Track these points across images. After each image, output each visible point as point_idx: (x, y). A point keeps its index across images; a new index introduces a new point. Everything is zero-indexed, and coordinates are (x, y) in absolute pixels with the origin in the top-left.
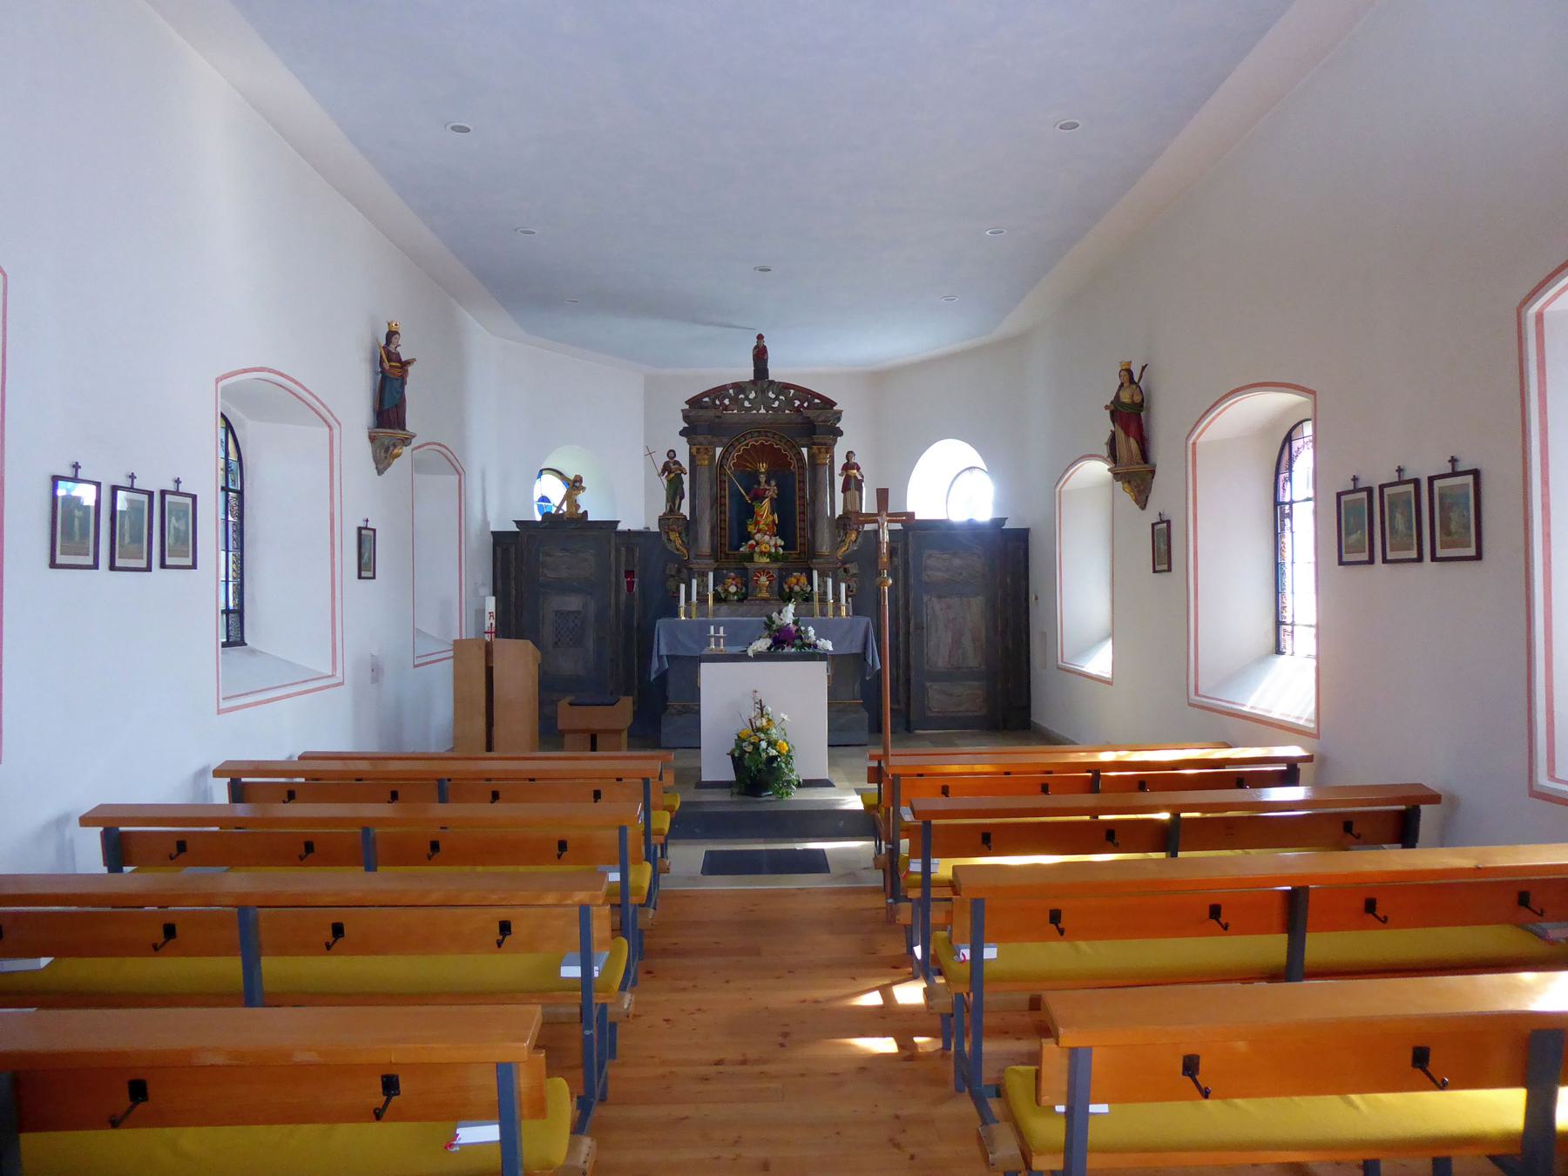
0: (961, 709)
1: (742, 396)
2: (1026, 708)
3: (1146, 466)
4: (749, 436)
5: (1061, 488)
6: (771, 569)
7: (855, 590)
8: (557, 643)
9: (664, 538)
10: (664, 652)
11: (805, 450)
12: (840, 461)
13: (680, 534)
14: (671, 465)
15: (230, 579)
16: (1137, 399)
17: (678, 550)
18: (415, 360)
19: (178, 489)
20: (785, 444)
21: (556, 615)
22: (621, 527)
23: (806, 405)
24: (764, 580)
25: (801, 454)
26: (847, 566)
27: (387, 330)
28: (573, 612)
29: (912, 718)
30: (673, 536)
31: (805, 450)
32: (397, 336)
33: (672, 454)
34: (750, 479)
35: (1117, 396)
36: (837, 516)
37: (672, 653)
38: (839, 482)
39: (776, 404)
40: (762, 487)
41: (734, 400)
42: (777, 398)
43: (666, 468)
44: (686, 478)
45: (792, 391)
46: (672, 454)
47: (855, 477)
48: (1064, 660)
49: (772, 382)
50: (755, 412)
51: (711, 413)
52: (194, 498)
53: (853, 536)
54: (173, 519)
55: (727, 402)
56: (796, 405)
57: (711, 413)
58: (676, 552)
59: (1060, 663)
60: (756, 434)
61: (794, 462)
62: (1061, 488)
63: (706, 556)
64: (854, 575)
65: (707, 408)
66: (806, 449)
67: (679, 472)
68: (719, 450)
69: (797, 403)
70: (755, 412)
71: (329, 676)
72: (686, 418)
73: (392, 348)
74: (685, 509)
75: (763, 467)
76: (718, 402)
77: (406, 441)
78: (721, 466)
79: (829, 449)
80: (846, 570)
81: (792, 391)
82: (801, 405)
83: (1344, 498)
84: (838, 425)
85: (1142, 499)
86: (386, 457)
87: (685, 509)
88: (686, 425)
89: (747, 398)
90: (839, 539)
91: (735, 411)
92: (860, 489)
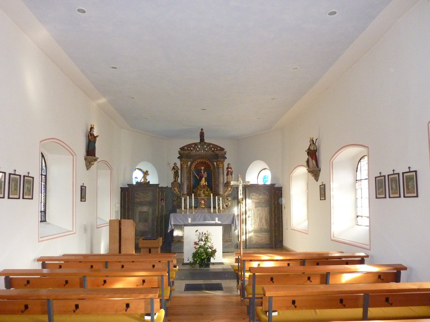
0: (262, 241)
1: (196, 147)
2: (282, 241)
3: (318, 168)
4: (198, 159)
5: (292, 175)
6: (205, 199)
7: (230, 205)
8: (140, 221)
9: (173, 189)
10: (172, 223)
11: (215, 163)
12: (226, 166)
13: (178, 188)
14: (175, 167)
15: (42, 201)
16: (315, 149)
17: (177, 193)
18: (98, 136)
19: (29, 175)
20: (209, 161)
21: (140, 212)
22: (276, 186)
23: (216, 149)
24: (203, 202)
25: (214, 164)
26: (228, 198)
27: (91, 127)
28: (145, 212)
29: (247, 244)
30: (176, 189)
31: (215, 163)
32: (93, 129)
33: (175, 164)
34: (198, 172)
35: (309, 148)
36: (225, 183)
37: (175, 224)
38: (225, 173)
39: (207, 149)
40: (202, 174)
41: (194, 148)
42: (207, 148)
43: (174, 168)
44: (179, 171)
45: (211, 146)
46: (175, 164)
47: (230, 171)
48: (334, 237)
49: (205, 143)
50: (200, 152)
51: (187, 152)
52: (33, 178)
53: (230, 189)
54: (27, 184)
55: (192, 148)
56: (213, 150)
57: (187, 152)
58: (176, 193)
59: (332, 238)
60: (201, 158)
61: (212, 167)
62: (292, 175)
63: (185, 195)
64: (230, 201)
65: (186, 150)
66: (215, 163)
67: (177, 169)
68: (189, 163)
69: (213, 149)
70: (200, 152)
71: (72, 231)
72: (180, 153)
73: (92, 132)
74: (179, 181)
75: (203, 168)
76: (189, 149)
77: (96, 160)
78: (190, 168)
79: (223, 163)
80: (227, 199)
81: (211, 146)
82: (214, 149)
83: (377, 179)
84: (225, 156)
85: (317, 179)
86: (89, 165)
87: (179, 181)
88: (180, 156)
89: (198, 147)
90: (225, 190)
91: (194, 151)
92: (232, 175)
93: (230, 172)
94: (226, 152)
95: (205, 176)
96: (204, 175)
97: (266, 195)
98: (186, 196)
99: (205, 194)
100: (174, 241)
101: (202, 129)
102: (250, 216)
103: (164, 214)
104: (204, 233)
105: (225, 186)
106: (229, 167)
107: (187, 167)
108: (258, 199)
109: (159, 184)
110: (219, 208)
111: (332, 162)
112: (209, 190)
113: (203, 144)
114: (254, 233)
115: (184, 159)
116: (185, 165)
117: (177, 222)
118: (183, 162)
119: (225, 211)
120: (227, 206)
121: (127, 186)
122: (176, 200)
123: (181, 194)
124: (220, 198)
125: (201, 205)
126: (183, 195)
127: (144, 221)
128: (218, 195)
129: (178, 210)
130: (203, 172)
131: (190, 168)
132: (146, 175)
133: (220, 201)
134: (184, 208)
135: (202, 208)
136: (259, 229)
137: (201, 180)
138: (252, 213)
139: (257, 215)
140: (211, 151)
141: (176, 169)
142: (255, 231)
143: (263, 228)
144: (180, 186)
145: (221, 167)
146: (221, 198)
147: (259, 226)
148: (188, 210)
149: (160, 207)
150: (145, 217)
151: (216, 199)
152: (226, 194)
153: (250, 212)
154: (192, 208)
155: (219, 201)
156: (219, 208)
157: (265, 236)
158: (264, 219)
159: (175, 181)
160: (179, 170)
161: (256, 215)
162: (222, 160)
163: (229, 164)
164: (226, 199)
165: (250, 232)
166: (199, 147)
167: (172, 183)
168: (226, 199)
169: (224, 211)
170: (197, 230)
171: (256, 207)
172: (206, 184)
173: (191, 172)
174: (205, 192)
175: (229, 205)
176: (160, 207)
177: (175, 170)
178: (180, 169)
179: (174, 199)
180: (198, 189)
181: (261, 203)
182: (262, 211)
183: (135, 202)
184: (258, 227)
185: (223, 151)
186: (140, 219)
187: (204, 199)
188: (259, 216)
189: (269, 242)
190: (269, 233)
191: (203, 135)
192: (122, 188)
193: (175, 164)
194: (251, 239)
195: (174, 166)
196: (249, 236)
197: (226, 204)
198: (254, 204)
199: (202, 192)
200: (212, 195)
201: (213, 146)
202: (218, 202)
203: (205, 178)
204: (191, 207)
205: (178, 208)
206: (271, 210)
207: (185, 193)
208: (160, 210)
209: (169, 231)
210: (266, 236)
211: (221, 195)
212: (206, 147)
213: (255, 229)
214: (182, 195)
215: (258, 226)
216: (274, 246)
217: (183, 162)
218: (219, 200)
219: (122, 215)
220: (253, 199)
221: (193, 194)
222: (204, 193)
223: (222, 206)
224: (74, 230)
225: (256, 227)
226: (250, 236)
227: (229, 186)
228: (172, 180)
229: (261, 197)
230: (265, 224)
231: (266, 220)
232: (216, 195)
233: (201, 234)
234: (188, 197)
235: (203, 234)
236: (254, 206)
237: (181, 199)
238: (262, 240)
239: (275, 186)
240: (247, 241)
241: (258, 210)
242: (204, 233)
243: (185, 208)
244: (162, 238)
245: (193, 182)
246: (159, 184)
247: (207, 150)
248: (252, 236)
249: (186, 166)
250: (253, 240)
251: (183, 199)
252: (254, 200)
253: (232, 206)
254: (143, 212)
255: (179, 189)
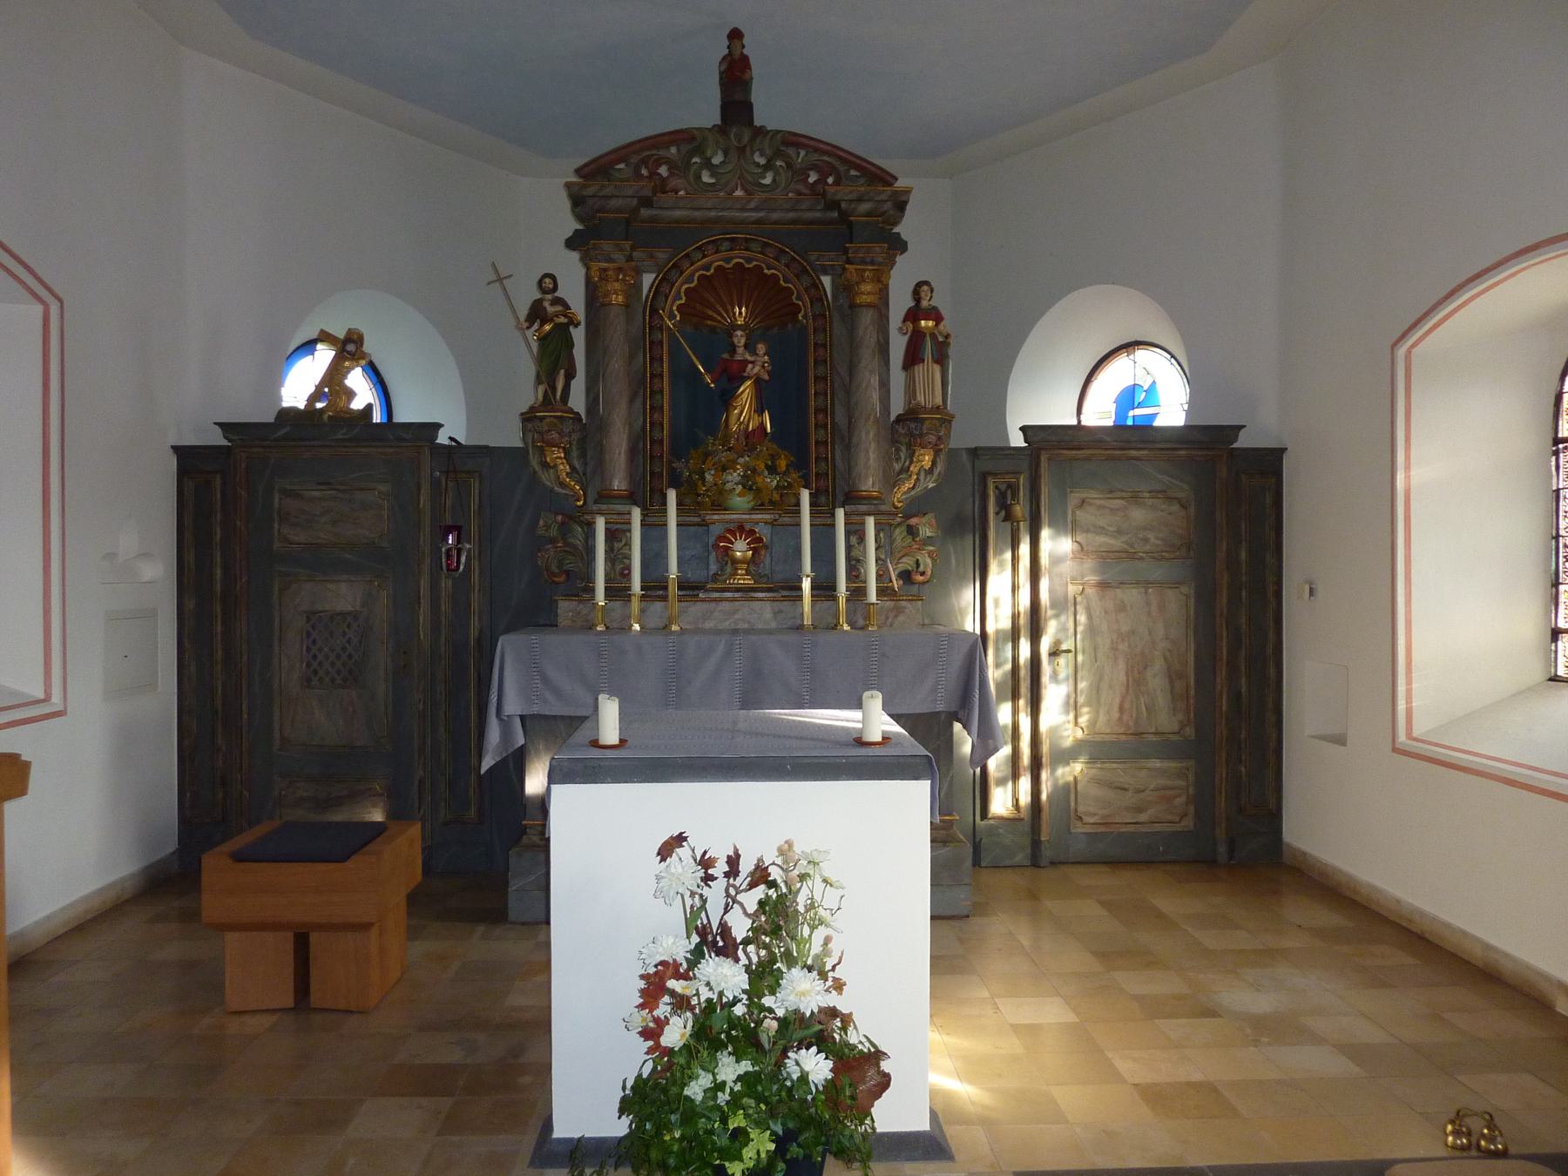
0: (1143, 817)
2: (1273, 816)
7: (929, 572)
8: (309, 680)
10: (513, 706)
12: (900, 302)
13: (567, 452)
14: (546, 304)
17: (562, 485)
20: (787, 266)
22: (1244, 441)
25: (817, 285)
26: (914, 521)
28: (343, 614)
31: (826, 281)
33: (548, 284)
34: (714, 343)
36: (893, 418)
37: (535, 710)
38: (898, 345)
40: (738, 358)
42: (768, 166)
43: (536, 313)
44: (578, 335)
46: (548, 284)
49: (761, 132)
53: (927, 460)
55: (663, 171)
59: (1402, 737)
62: (1413, 346)
64: (929, 541)
67: (563, 320)
68: (648, 279)
69: (813, 178)
78: (654, 311)
81: (802, 153)
82: (822, 181)
89: (707, 164)
90: (897, 467)
93: (928, 338)
94: (908, 192)
95: (757, 369)
96: (752, 362)
97: (1175, 507)
98: (619, 508)
99: (759, 490)
100: (525, 839)
101: (735, 35)
102: (1064, 647)
103: (474, 633)
104: (746, 866)
105: (894, 442)
106: (924, 303)
107: (627, 306)
108: (1120, 532)
109: (442, 426)
110: (857, 593)
111: (1409, 352)
112: (782, 464)
113: (746, 139)
114: (1092, 760)
115: (607, 246)
116: (617, 286)
117: (550, 697)
118: (605, 270)
119: (899, 611)
120: (906, 576)
121: (217, 439)
122: (554, 532)
123: (592, 496)
124: (863, 524)
125: (729, 569)
126: (605, 496)
127: (339, 681)
128: (851, 498)
129: (565, 607)
130: (746, 346)
131: (654, 311)
132: (346, 359)
133: (862, 539)
134: (610, 593)
135: (738, 590)
136: (1123, 738)
137: (727, 398)
138: (1080, 629)
139: (1112, 642)
140: (800, 187)
141: (551, 320)
142: (1095, 749)
143: (1153, 730)
144: (583, 442)
145: (869, 306)
146: (870, 522)
147: (1125, 718)
148: (635, 604)
149: (446, 584)
150: (344, 649)
151: (833, 526)
152: (902, 493)
153: (1063, 618)
154: (665, 588)
155: (854, 540)
156: (857, 593)
157: (1161, 782)
158: (1158, 665)
159: (547, 402)
160: (577, 325)
161: (1104, 642)
162: (879, 251)
163: (925, 288)
164: (903, 528)
165: (1064, 756)
166: (717, 160)
167: (528, 418)
168: (899, 533)
169: (891, 615)
170: (680, 839)
171: (1103, 586)
172: (762, 426)
173: (661, 343)
174: (759, 480)
175: (921, 569)
176: (446, 584)
177: (547, 327)
178: (581, 317)
179: (541, 532)
180: (707, 455)
181: (1141, 559)
182: (1149, 613)
183: (276, 545)
184: (1120, 719)
185: (890, 185)
186: (315, 664)
187: (747, 527)
188: (1123, 647)
189: (1188, 824)
190: (1191, 763)
191: (747, 76)
192: (183, 453)
193: (548, 282)
194: (1073, 804)
195: (538, 296)
196: (1055, 786)
197: (901, 567)
198: (1089, 564)
199: (734, 477)
200: (805, 496)
201: (815, 157)
202: (849, 548)
203: (758, 382)
204: (655, 587)
205: (572, 594)
206: (1205, 599)
207: (619, 483)
208: (444, 606)
209: (487, 763)
210: (1169, 783)
211: (870, 498)
212: (762, 161)
213: (1098, 738)
214: (596, 502)
215: (1116, 715)
216: (1222, 849)
217: (605, 265)
218: (855, 532)
219: (186, 640)
220: (1088, 531)
221: (672, 496)
222: (748, 484)
223: (879, 577)
224: (56, 698)
225: (1102, 718)
226: (1061, 782)
227: (921, 436)
228: (527, 394)
229: (1138, 515)
230: (1162, 701)
231: (1173, 675)
232: (834, 496)
233: (720, 868)
234: (636, 514)
235: (742, 880)
236: (1092, 578)
237: (590, 527)
238: (1139, 810)
239: (1235, 439)
240: (1045, 815)
241: (1121, 608)
242: (746, 866)
243: (617, 591)
244: (419, 826)
245: (671, 408)
246: (442, 426)
247: (774, 180)
248: (1075, 778)
249: (620, 298)
250: (1081, 809)
251: (600, 525)
252: (1090, 536)
253: (944, 581)
254: (332, 618)
255: (577, 464)
